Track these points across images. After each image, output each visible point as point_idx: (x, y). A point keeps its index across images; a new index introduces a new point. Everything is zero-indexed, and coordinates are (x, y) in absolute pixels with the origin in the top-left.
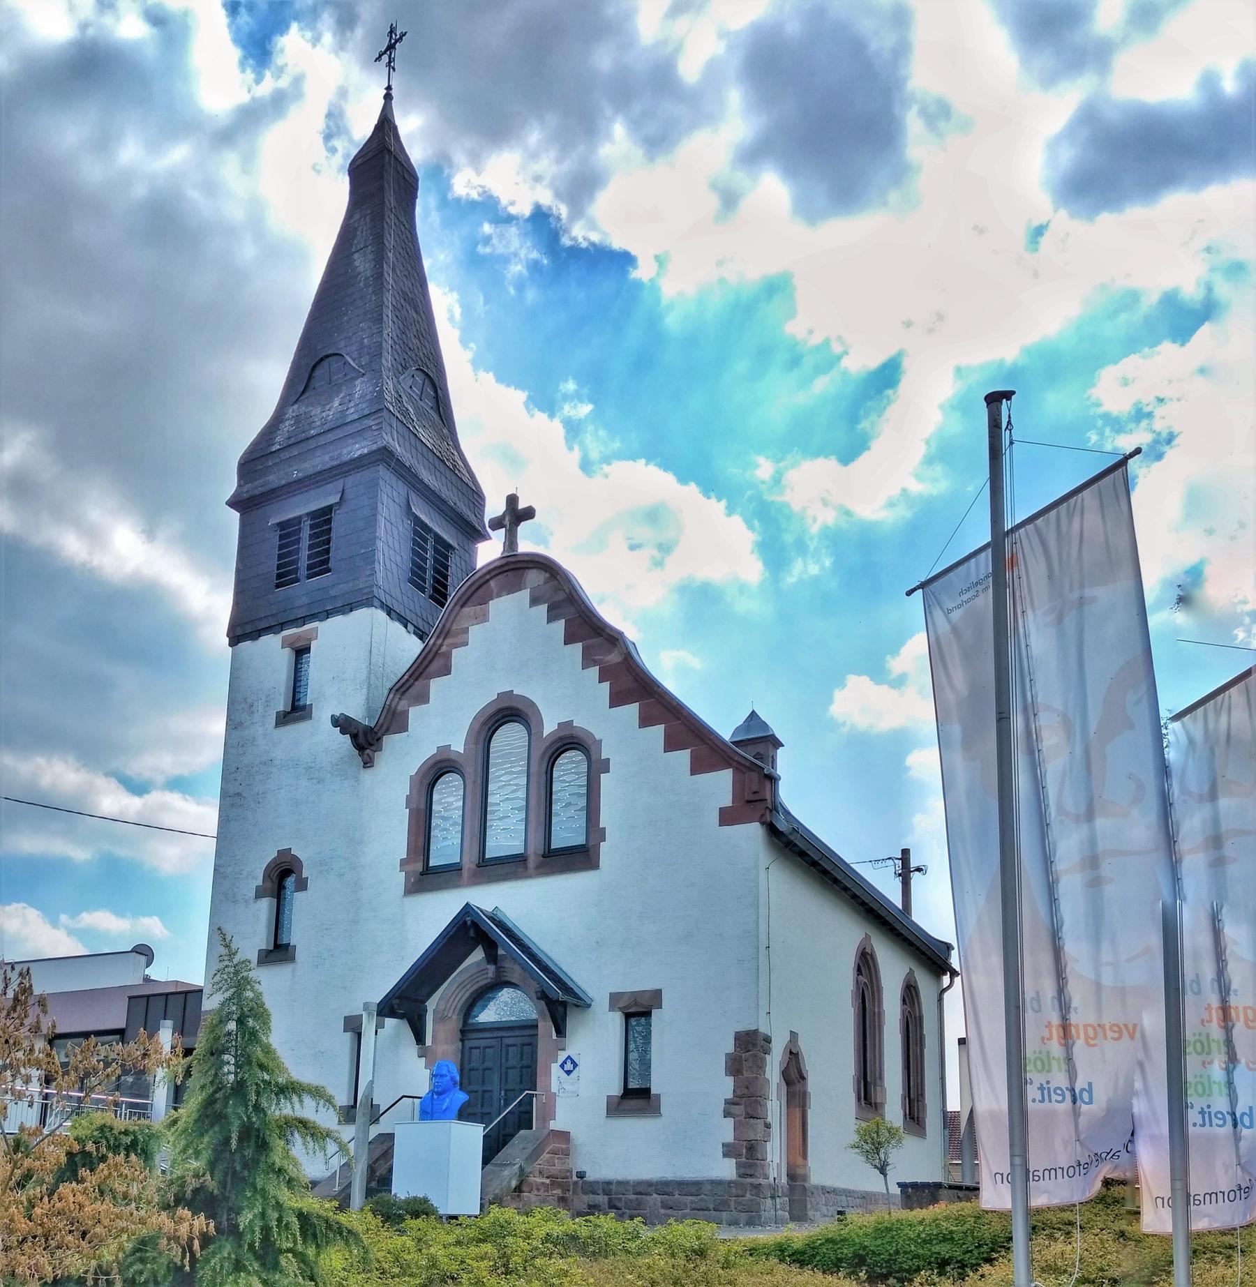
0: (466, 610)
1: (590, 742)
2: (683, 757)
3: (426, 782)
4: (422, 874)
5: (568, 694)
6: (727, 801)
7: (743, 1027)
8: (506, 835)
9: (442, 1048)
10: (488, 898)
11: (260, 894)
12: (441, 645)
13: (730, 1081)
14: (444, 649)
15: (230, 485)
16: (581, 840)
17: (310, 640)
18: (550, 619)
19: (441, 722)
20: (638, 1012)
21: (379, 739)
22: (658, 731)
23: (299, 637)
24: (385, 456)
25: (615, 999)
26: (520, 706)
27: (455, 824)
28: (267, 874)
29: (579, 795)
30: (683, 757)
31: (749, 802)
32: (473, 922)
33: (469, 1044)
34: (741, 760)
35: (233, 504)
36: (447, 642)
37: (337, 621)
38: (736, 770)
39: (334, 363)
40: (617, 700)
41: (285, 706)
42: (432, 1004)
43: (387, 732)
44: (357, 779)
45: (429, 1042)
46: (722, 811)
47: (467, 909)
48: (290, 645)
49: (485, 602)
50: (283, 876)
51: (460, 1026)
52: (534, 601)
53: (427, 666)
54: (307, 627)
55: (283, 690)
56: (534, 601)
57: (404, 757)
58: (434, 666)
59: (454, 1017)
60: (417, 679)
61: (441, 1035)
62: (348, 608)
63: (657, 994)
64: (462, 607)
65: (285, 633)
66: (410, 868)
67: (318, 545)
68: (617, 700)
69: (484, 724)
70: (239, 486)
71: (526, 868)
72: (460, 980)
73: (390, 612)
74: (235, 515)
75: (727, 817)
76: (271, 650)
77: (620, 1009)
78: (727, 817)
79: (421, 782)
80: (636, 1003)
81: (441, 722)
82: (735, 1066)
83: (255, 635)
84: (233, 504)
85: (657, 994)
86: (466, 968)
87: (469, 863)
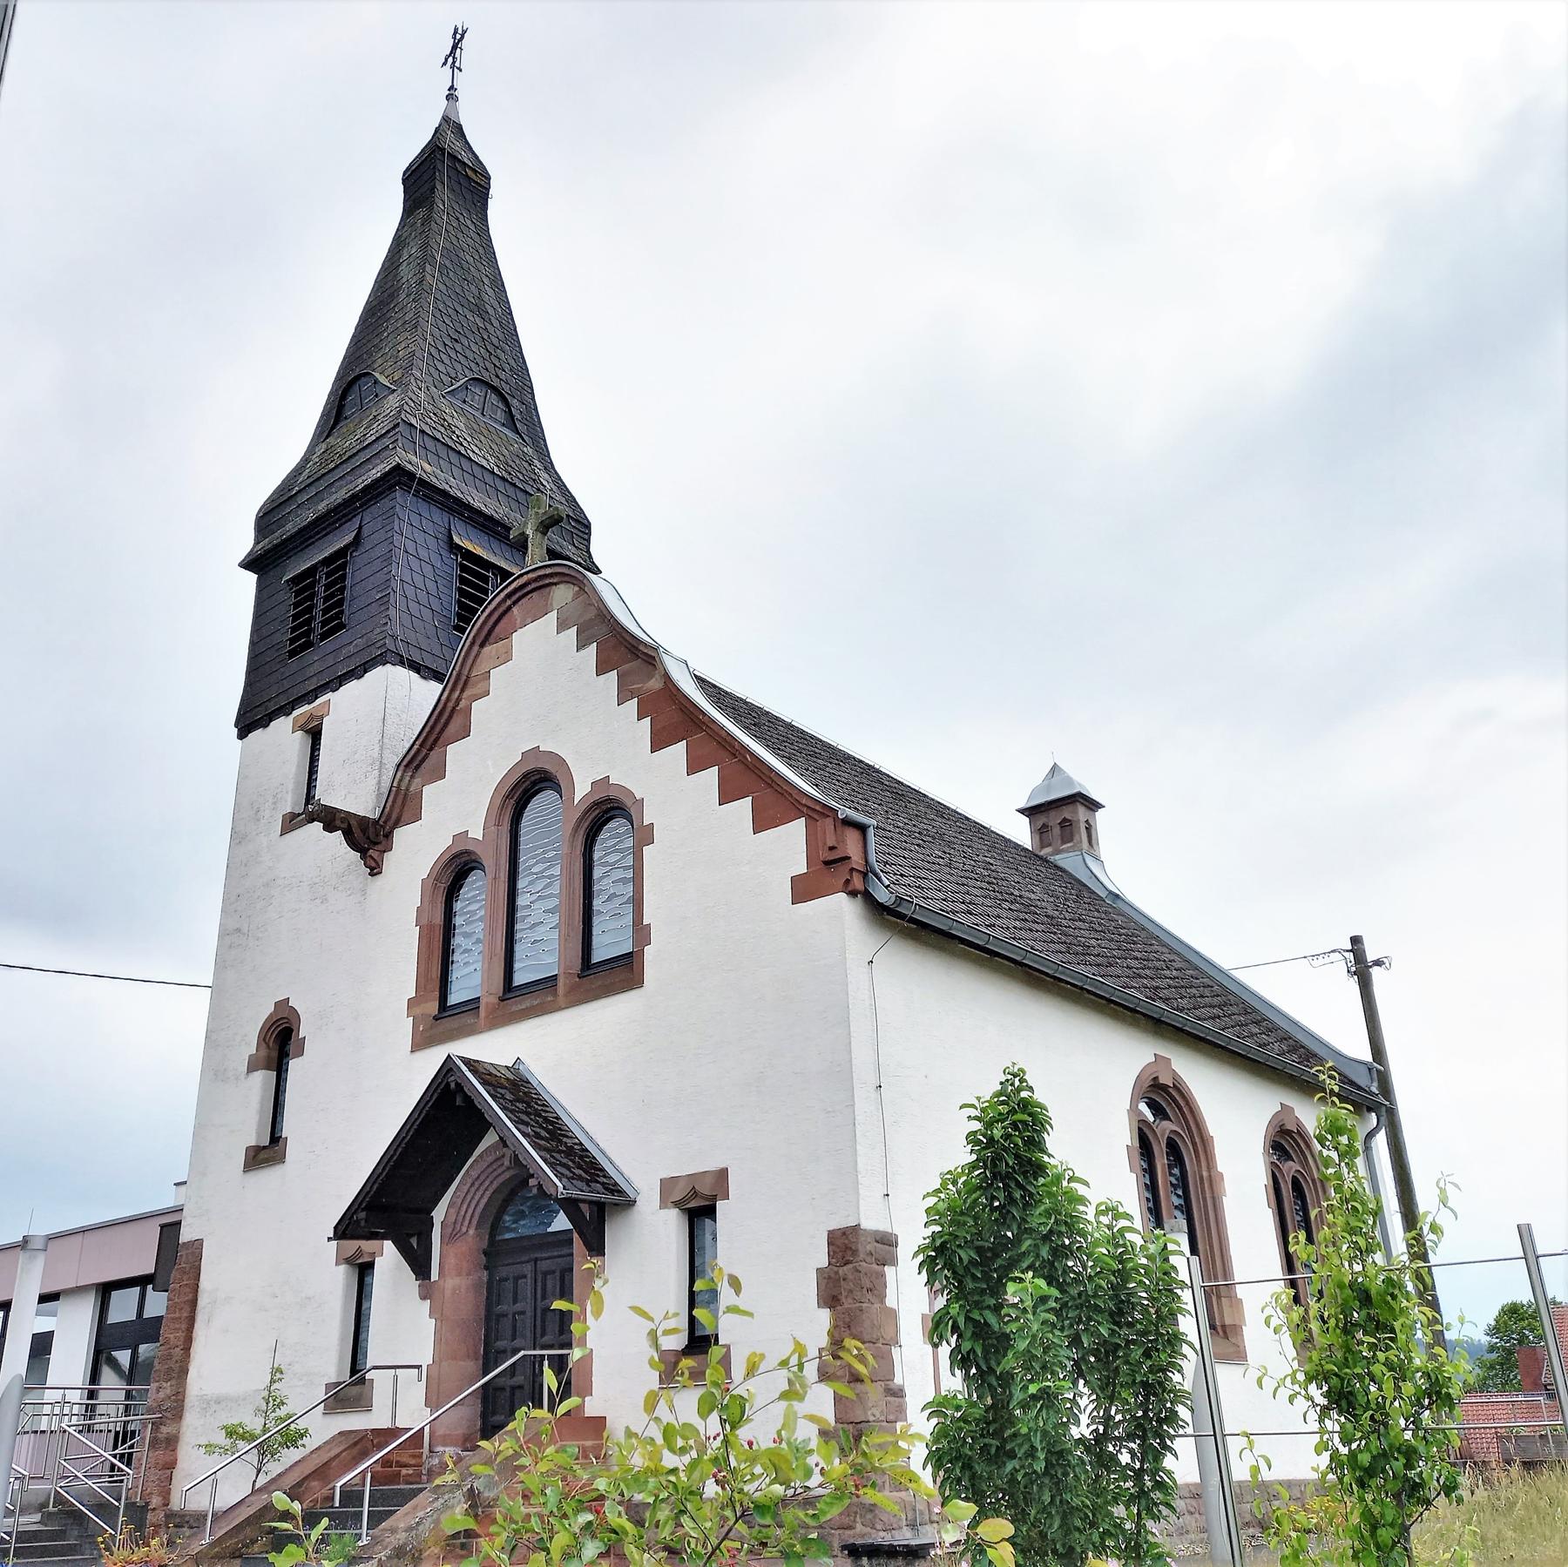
0: (487, 649)
1: (628, 802)
2: (743, 808)
3: (443, 886)
4: (436, 1018)
5: (605, 743)
6: (800, 865)
7: (838, 1223)
8: (543, 950)
9: (451, 1283)
10: (494, 1047)
11: (252, 1068)
12: (458, 700)
13: (824, 1317)
14: (462, 704)
15: (244, 541)
16: (627, 947)
17: (322, 717)
18: (581, 646)
19: (459, 806)
20: (699, 1208)
21: (389, 836)
22: (711, 776)
23: (311, 717)
24: (400, 477)
25: (667, 1185)
26: (547, 767)
27: (478, 941)
28: (263, 1038)
29: (624, 881)
30: (743, 808)
31: (827, 863)
32: (457, 1084)
33: (503, 1271)
34: (810, 804)
35: (250, 564)
36: (465, 695)
37: (351, 688)
38: (809, 818)
39: (366, 385)
40: (659, 742)
41: (295, 804)
42: (439, 1214)
43: (397, 824)
44: (364, 892)
45: (434, 1276)
46: (795, 880)
47: (448, 1067)
48: (302, 728)
49: (508, 636)
50: (281, 1041)
51: (485, 1245)
52: (562, 626)
53: (442, 730)
54: (318, 702)
55: (291, 786)
56: (562, 626)
57: (416, 852)
58: (452, 728)
59: (471, 1232)
60: (431, 749)
61: (452, 1261)
62: (358, 672)
63: (723, 1174)
64: (482, 645)
65: (296, 713)
66: (418, 1011)
67: (332, 595)
68: (659, 742)
69: (508, 797)
70: (257, 542)
71: (555, 994)
72: (474, 1174)
73: (415, 667)
74: (251, 578)
75: (803, 890)
76: (283, 734)
77: (676, 1204)
78: (803, 890)
79: (435, 887)
80: (695, 1193)
81: (459, 806)
82: (831, 1294)
83: (264, 722)
84: (250, 564)
85: (723, 1174)
86: (481, 1156)
87: (488, 1001)
